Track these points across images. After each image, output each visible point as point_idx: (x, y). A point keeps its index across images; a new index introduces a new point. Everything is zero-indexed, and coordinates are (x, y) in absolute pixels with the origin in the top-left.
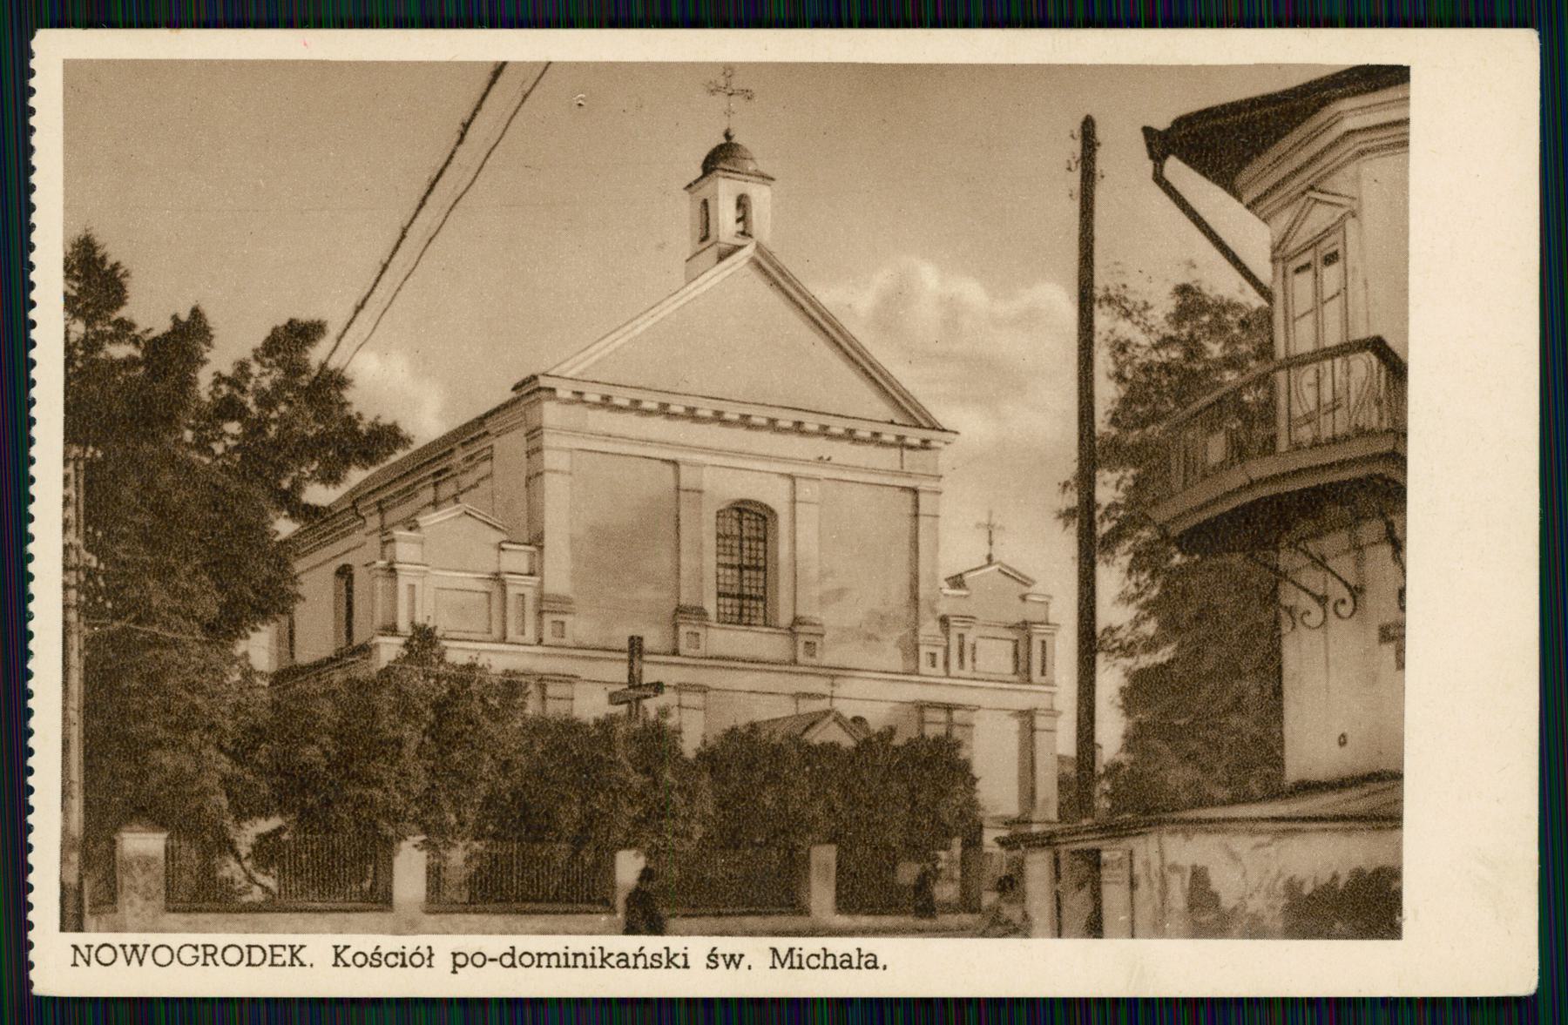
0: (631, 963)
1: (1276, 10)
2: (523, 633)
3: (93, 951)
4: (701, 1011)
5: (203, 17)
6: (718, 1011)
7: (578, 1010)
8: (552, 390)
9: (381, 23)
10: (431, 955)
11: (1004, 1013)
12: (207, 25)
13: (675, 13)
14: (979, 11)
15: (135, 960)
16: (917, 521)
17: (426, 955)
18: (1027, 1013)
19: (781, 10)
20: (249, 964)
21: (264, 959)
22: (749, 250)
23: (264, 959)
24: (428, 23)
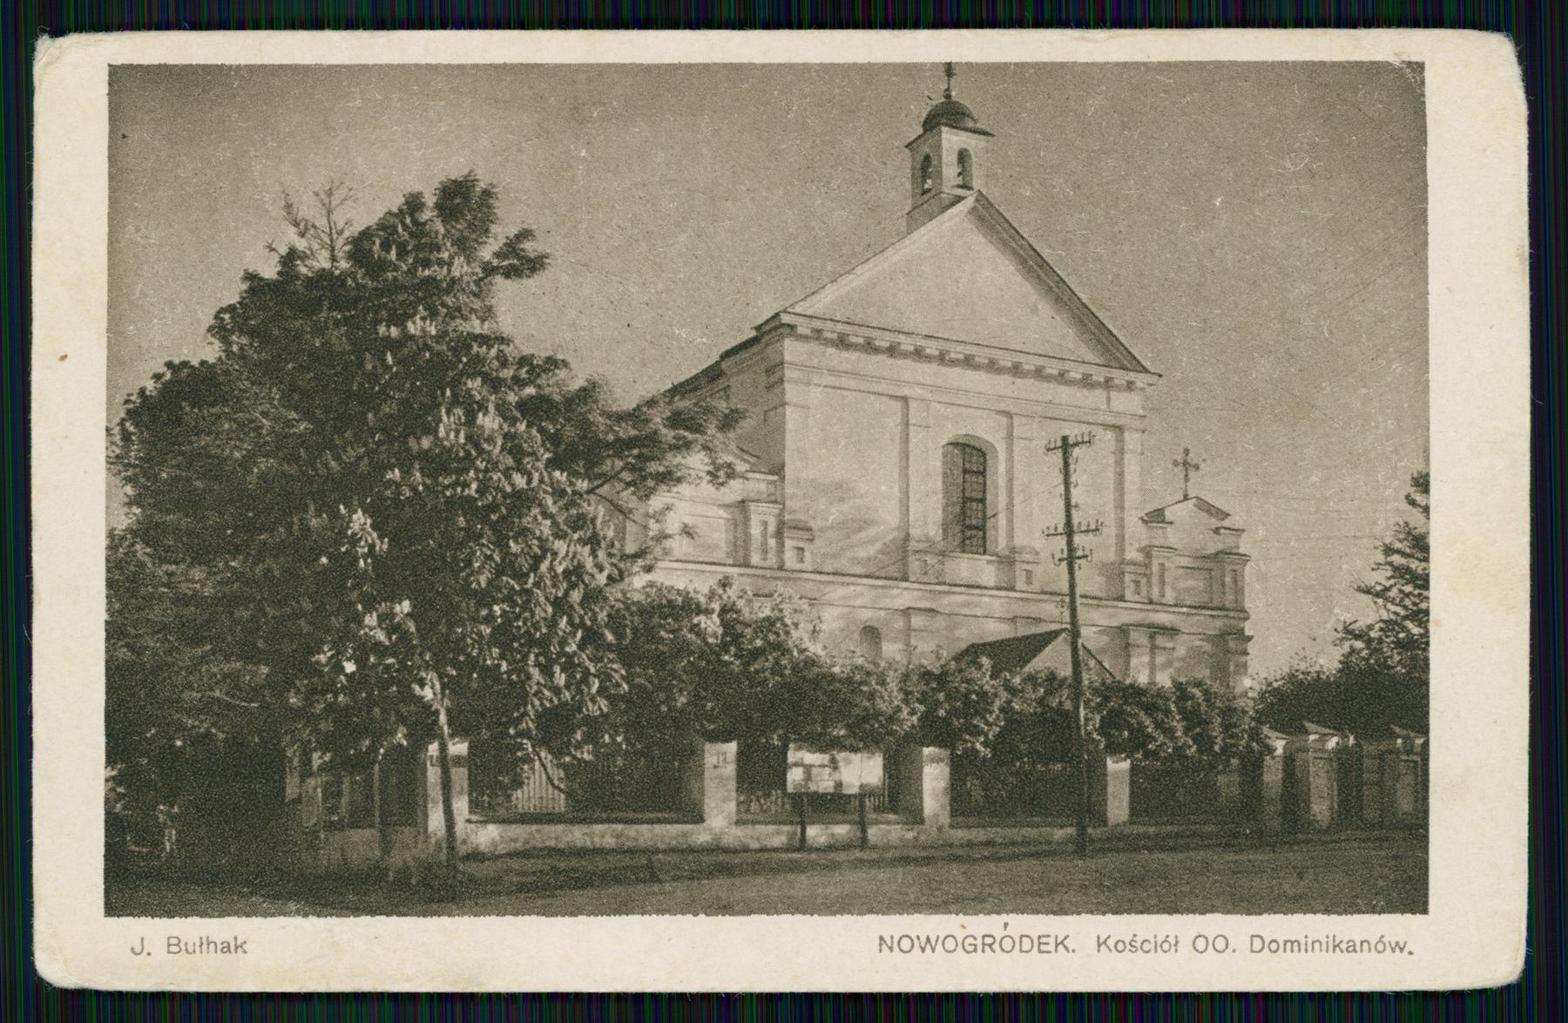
0: (1358, 948)
1: (1225, 11)
2: (802, 561)
3: (896, 941)
4: (630, 1006)
5: (155, 18)
6: (648, 1006)
7: (508, 1006)
8: (792, 327)
9: (332, 24)
10: (1177, 942)
11: (933, 1008)
12: (159, 27)
13: (626, 13)
14: (929, 13)
15: (928, 948)
16: (1012, 444)
17: (1173, 942)
18: (956, 1012)
19: (729, 10)
20: (1021, 951)
21: (899, 942)
22: (969, 202)
23: (899, 942)
24: (380, 24)
